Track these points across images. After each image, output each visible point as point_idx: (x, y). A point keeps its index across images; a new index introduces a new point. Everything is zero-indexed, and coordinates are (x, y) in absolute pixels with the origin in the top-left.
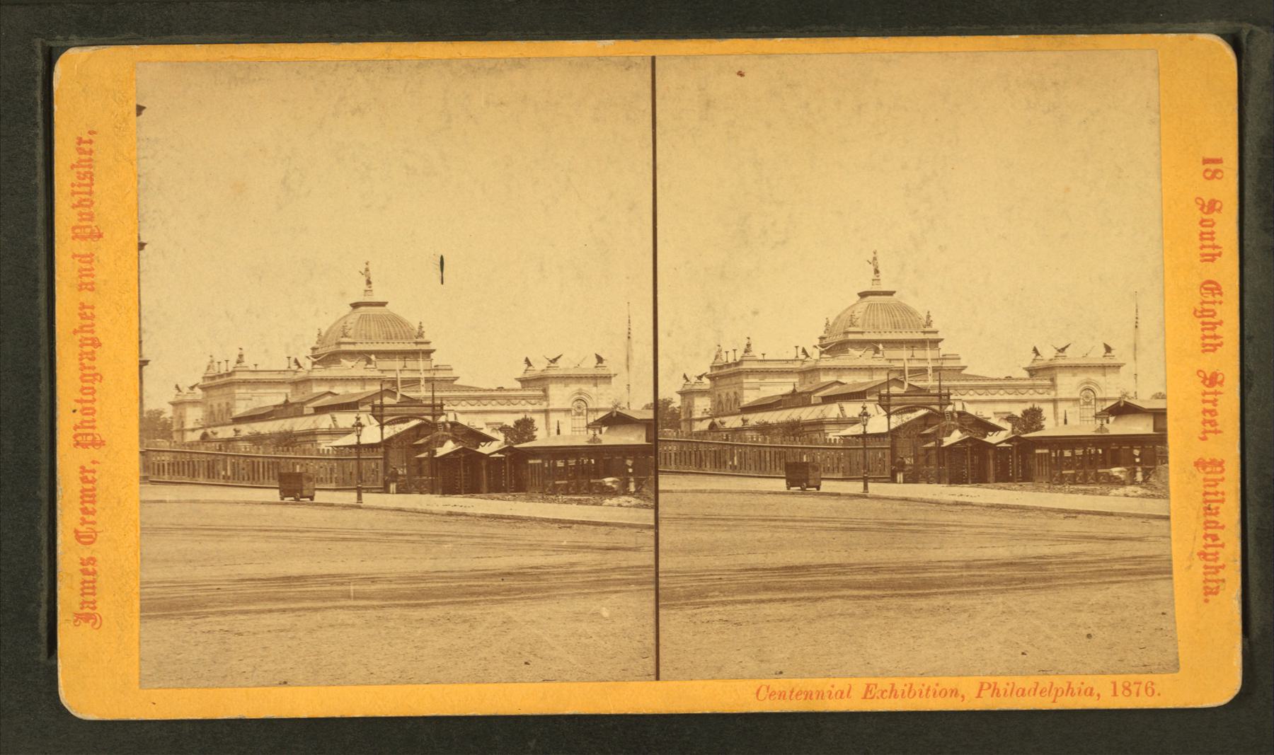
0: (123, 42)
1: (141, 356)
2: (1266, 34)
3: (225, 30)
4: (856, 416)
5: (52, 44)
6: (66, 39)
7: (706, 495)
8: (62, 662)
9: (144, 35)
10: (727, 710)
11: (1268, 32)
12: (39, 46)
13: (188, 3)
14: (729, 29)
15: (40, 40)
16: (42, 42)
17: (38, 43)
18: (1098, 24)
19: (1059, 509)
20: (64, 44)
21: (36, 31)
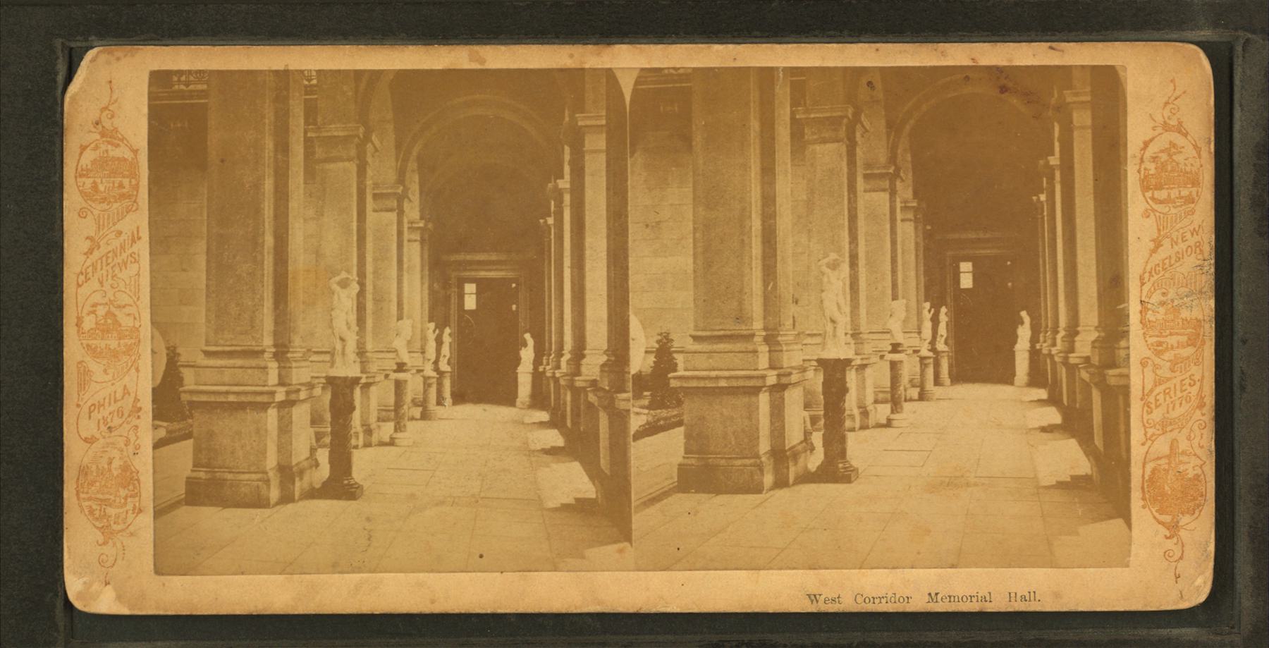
0: (141, 43)
1: (835, 328)
2: (1261, 41)
3: (242, 31)
4: (196, 414)
5: (73, 45)
6: (86, 40)
7: (77, 502)
8: (69, 552)
9: (163, 37)
10: (530, 610)
11: (1264, 40)
12: (59, 47)
13: (206, 5)
14: (736, 34)
15: (61, 40)
16: (62, 43)
17: (58, 43)
18: (1097, 31)
19: (1050, 426)
20: (84, 44)
21: (57, 32)
